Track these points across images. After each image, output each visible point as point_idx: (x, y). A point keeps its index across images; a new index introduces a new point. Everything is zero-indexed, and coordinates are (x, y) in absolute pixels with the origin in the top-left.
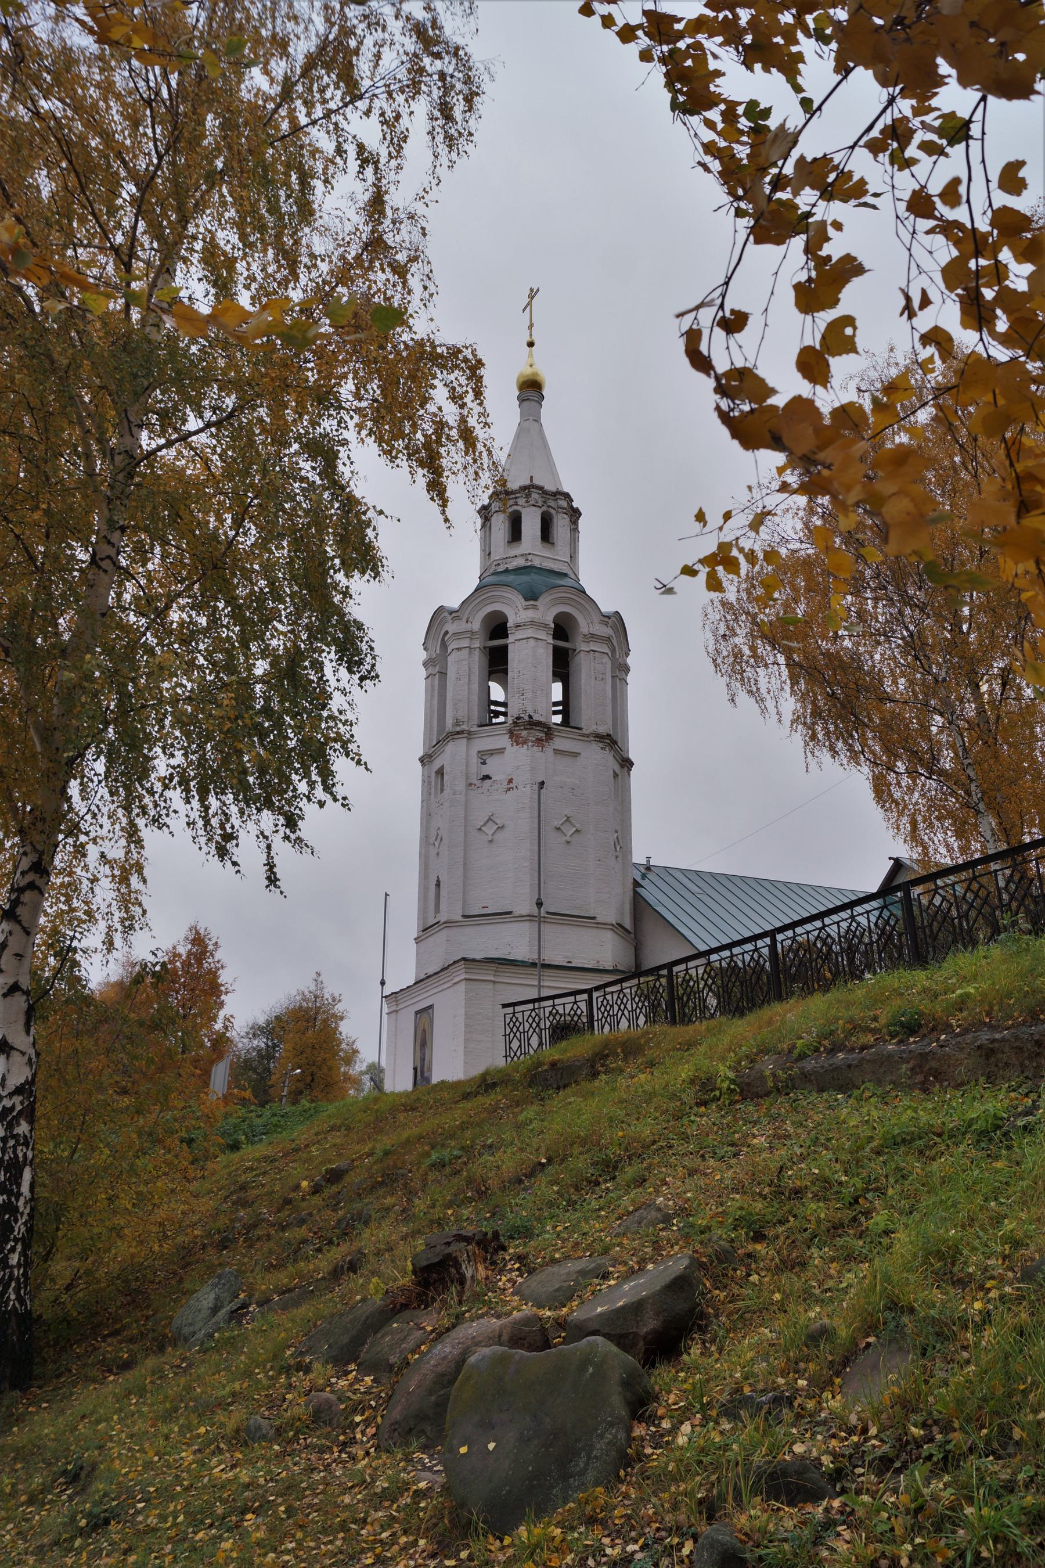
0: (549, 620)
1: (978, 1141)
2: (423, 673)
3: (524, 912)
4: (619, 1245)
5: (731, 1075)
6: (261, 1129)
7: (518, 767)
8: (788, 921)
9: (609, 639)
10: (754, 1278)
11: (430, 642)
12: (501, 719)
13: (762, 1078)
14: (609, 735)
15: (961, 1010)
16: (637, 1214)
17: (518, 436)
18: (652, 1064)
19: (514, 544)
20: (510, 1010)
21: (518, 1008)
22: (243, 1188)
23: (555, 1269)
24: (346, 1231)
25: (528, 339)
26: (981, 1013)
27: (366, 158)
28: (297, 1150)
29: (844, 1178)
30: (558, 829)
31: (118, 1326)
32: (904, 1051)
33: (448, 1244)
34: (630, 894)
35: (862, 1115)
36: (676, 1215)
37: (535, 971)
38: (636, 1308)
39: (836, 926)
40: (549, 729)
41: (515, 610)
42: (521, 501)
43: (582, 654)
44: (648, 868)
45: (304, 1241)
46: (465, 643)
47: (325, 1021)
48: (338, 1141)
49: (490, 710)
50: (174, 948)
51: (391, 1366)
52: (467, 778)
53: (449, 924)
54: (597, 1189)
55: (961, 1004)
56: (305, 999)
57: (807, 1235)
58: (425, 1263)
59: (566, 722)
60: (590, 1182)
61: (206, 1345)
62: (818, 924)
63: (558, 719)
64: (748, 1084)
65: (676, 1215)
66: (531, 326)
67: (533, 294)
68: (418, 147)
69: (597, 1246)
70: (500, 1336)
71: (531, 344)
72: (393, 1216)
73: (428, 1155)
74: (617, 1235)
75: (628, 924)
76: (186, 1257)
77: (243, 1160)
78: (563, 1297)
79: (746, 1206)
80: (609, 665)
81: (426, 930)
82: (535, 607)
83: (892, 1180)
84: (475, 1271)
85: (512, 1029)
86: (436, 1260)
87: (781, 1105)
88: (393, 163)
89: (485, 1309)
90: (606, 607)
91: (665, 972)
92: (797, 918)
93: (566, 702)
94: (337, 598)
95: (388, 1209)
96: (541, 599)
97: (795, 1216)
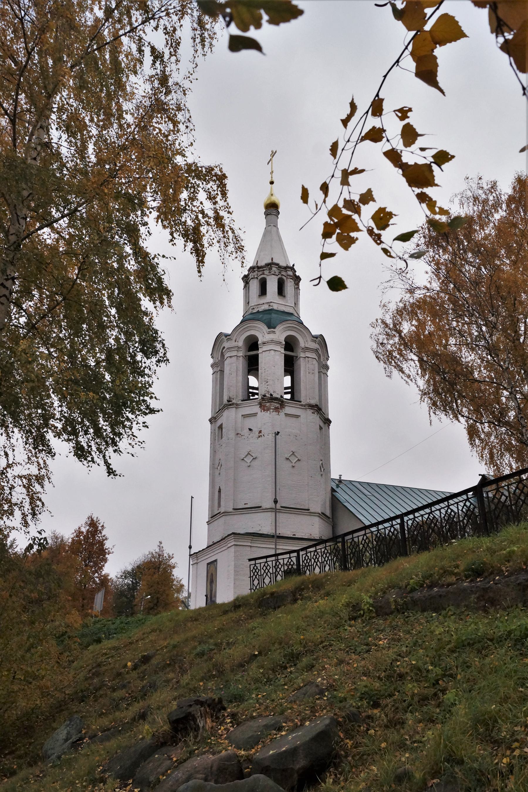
0: (282, 339)
1: (515, 645)
2: (211, 371)
3: (268, 507)
4: (291, 708)
5: (371, 601)
6: (113, 631)
7: (264, 424)
8: (410, 509)
9: (316, 351)
10: (372, 732)
12: (256, 397)
13: (388, 603)
14: (317, 405)
15: (509, 561)
16: (304, 688)
17: (264, 235)
18: (328, 594)
19: (263, 297)
20: (253, 562)
21: (258, 561)
22: (99, 665)
23: (251, 723)
24: (144, 694)
25: (270, 180)
26: (521, 563)
27: (157, 56)
28: (131, 643)
29: (430, 668)
30: (288, 459)
31: (14, 748)
32: (473, 586)
33: (190, 706)
34: (329, 496)
35: (444, 627)
36: (327, 690)
37: (273, 540)
38: (293, 752)
39: (439, 512)
40: (282, 402)
41: (262, 333)
42: (266, 272)
43: (301, 359)
44: (340, 481)
45: (122, 699)
46: (234, 353)
47: (165, 569)
48: (153, 638)
49: (249, 393)
50: (79, 528)
51: (150, 783)
52: (236, 430)
53: (226, 513)
54: (285, 671)
55: (509, 558)
56: (153, 557)
57: (405, 704)
58: (174, 718)
59: (292, 398)
60: (281, 667)
61: (56, 763)
62: (428, 510)
63: (288, 396)
64: (380, 607)
65: (327, 690)
66: (272, 172)
67: (273, 154)
68: (186, 49)
69: (278, 709)
70: (211, 767)
72: (171, 685)
73: (195, 648)
74: (291, 702)
75: (328, 513)
76: (60, 708)
77: (101, 649)
78: (253, 742)
79: (369, 685)
80: (317, 365)
81: (213, 517)
82: (274, 332)
83: (460, 670)
84: (206, 723)
85: (254, 573)
86: (182, 716)
87: (399, 620)
88: (173, 59)
89: (207, 748)
90: (315, 332)
91: (340, 540)
92: (415, 507)
93: (292, 387)
94: (146, 319)
95: (168, 681)
96: (277, 328)
97: (399, 692)
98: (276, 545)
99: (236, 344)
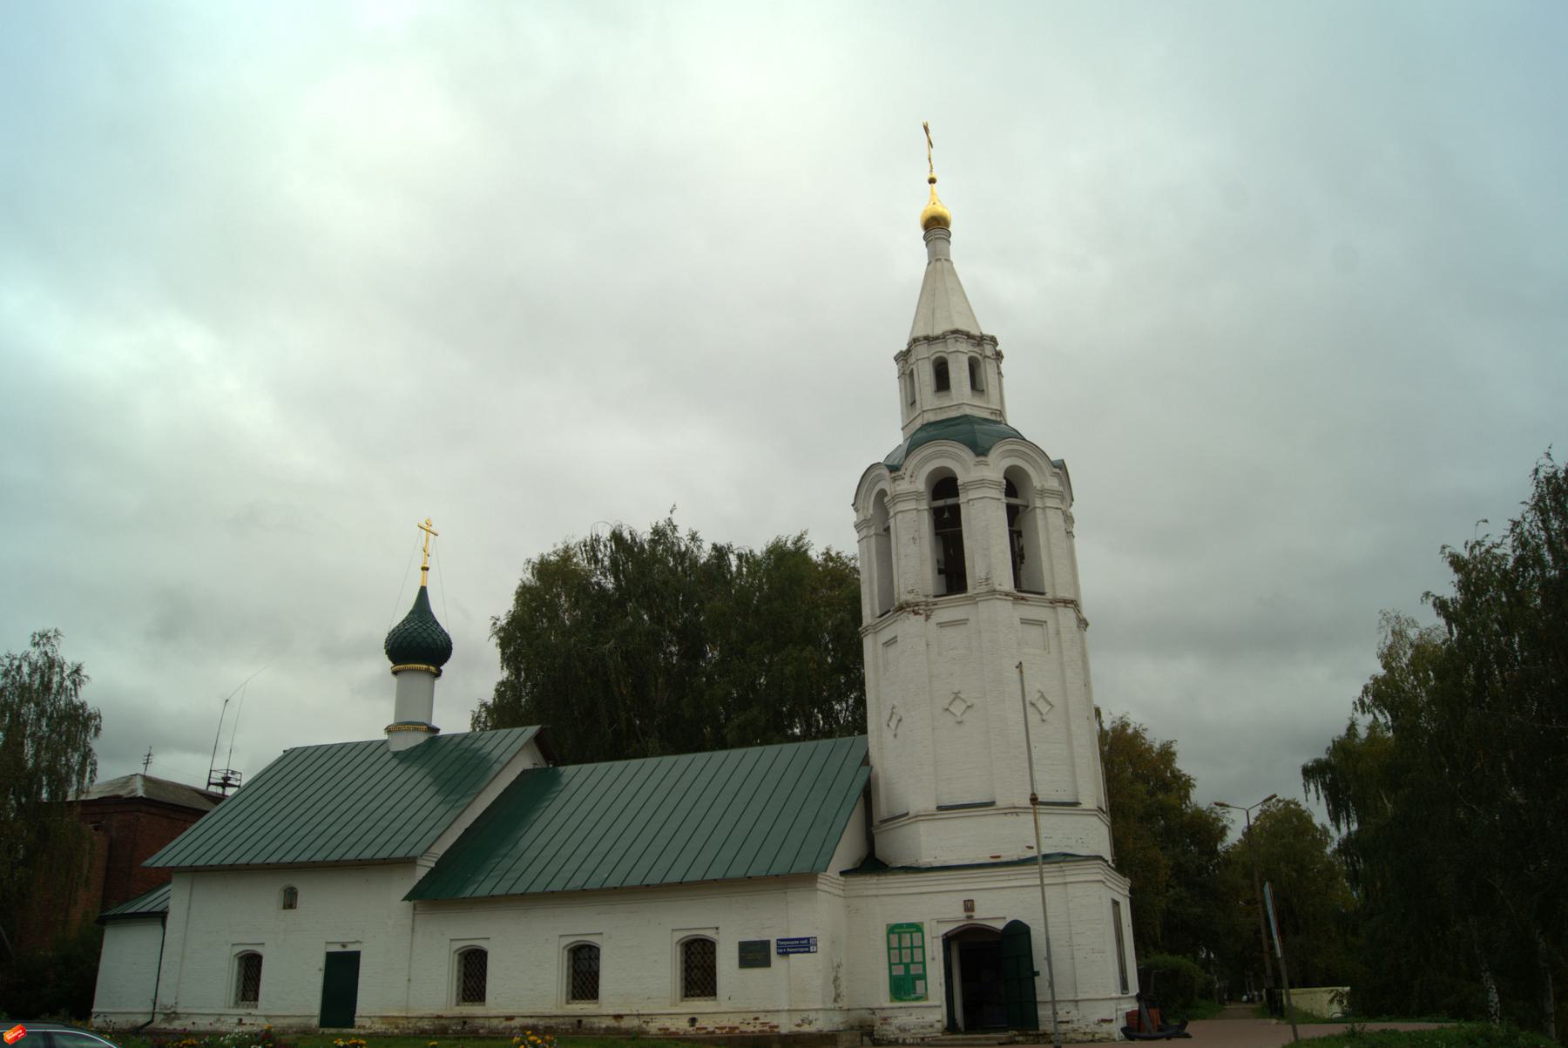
0: (998, 476)
11: (860, 501)
25: (928, 176)
37: (1029, 877)
41: (965, 467)
47: (1498, 567)
71: (932, 181)
98: (1042, 879)
99: (912, 488)
